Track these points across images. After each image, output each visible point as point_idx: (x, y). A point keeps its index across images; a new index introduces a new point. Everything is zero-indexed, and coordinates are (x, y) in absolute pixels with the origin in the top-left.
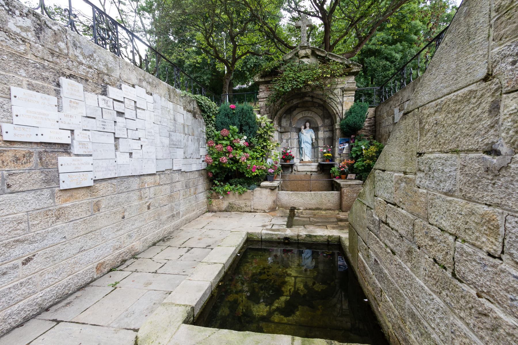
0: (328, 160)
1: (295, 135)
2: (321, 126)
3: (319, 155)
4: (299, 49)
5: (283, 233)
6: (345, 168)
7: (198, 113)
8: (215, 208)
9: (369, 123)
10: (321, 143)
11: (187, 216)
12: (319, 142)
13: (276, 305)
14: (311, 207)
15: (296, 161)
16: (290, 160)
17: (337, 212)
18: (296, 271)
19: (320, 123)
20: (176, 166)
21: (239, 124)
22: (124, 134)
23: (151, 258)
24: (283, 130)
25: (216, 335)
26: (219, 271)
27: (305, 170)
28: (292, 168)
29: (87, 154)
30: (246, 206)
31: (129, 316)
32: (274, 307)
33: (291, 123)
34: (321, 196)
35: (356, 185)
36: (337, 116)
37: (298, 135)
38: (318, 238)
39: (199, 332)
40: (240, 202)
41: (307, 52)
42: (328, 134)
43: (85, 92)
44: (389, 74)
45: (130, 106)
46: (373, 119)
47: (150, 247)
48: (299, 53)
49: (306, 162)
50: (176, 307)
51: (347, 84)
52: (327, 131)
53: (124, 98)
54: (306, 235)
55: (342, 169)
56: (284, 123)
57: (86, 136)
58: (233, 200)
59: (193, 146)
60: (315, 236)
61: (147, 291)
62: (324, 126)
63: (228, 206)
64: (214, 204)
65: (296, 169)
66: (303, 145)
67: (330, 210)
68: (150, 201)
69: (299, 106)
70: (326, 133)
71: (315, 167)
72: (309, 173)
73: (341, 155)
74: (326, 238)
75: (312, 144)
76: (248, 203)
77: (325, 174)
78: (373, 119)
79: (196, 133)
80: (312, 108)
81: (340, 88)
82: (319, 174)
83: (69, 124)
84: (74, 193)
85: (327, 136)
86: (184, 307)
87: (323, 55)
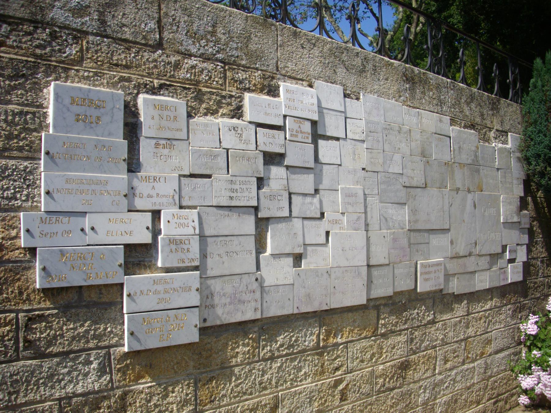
20: (426, 280)
22: (281, 208)
29: (187, 264)
43: (346, 99)
45: (300, 135)
53: (293, 284)
57: (186, 222)
68: (349, 377)
83: (150, 196)
84: (232, 208)
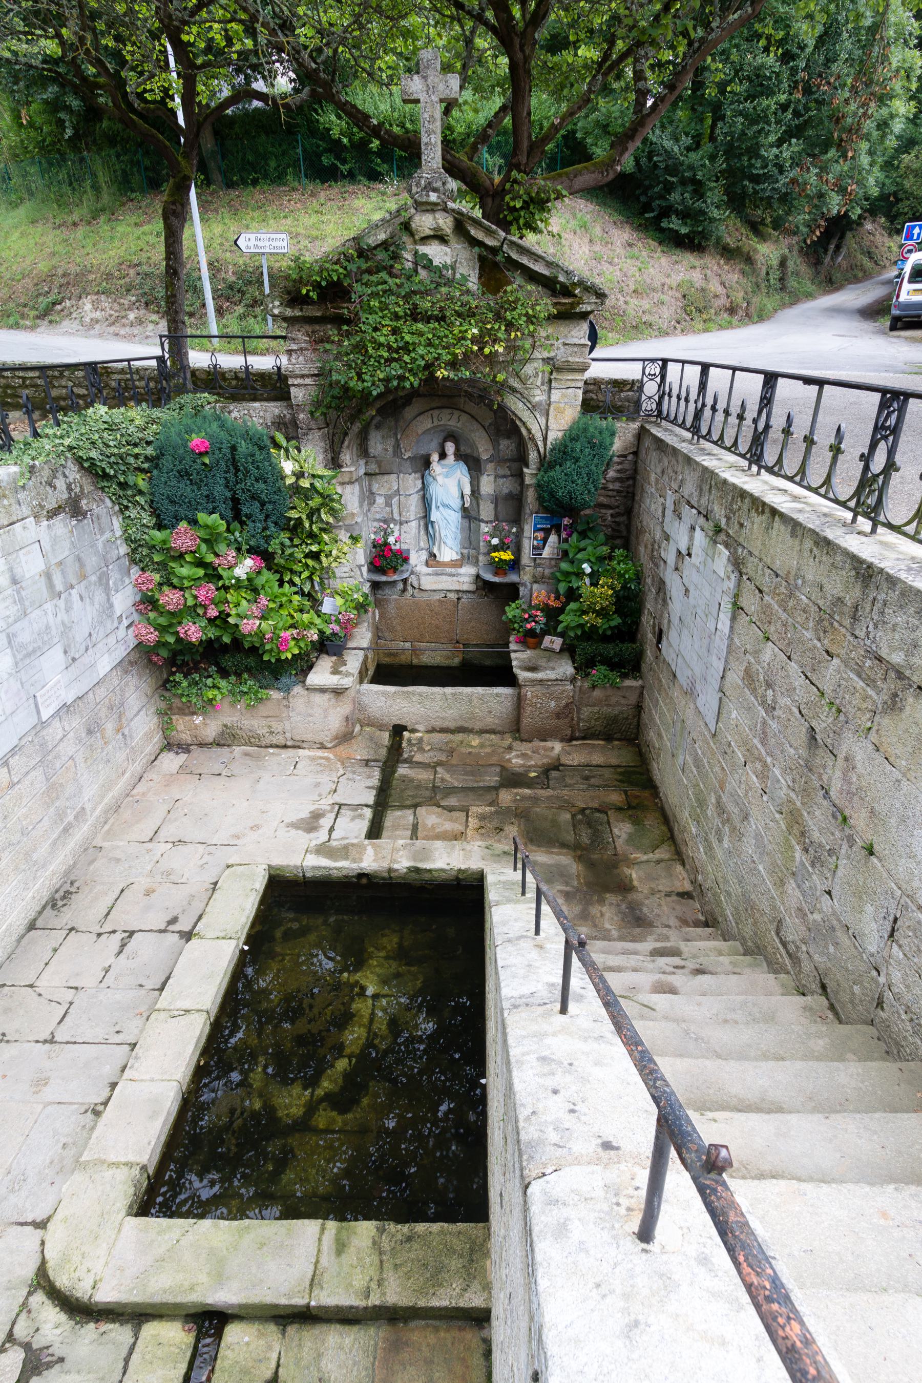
1: (412, 483)
2: (489, 461)
4: (413, 211)
5: (354, 866)
6: (536, 622)
7: (88, 488)
8: (186, 737)
9: (618, 471)
10: (487, 511)
11: (106, 800)
13: (326, 1085)
14: (444, 726)
15: (417, 559)
17: (508, 740)
18: (378, 976)
19: (484, 450)
21: (229, 495)
23: (31, 986)
24: (373, 468)
25: (189, 1236)
26: (195, 1040)
27: (440, 587)
30: (271, 733)
31: (17, 1188)
32: (320, 1092)
33: (397, 447)
34: (470, 701)
35: (557, 680)
36: (530, 445)
37: (423, 477)
38: (436, 874)
39: (159, 1233)
40: (255, 723)
41: (441, 222)
42: (507, 486)
44: (769, 106)
46: (630, 457)
47: (23, 936)
48: (413, 225)
49: (445, 565)
50: (111, 1172)
51: (562, 349)
52: (504, 476)
54: (408, 868)
55: (528, 626)
56: (378, 445)
58: (235, 719)
59: (88, 608)
60: (430, 871)
61: (41, 1106)
62: (497, 459)
63: (223, 733)
64: (181, 727)
65: (416, 584)
66: (435, 516)
67: (492, 732)
70: (501, 481)
71: (467, 579)
74: (455, 873)
75: (464, 510)
76: (276, 726)
78: (630, 457)
79: (92, 562)
82: (481, 596)
85: (506, 491)
86: (125, 1169)
87: (490, 242)
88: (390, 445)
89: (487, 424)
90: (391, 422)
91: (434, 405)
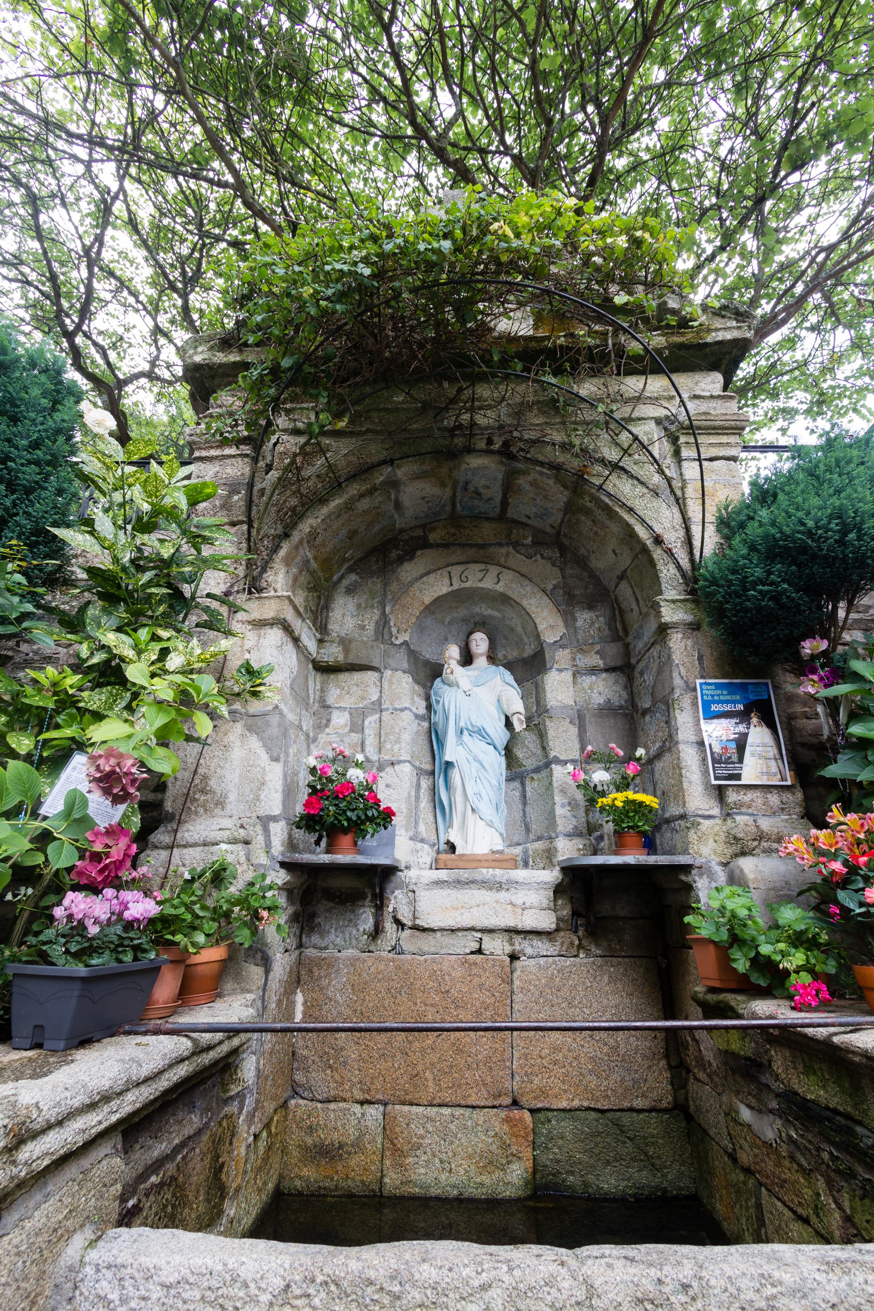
0: (632, 838)
2: (559, 644)
3: (560, 811)
12: (551, 733)
16: (357, 828)
24: (333, 653)
27: (466, 921)
28: (380, 904)
33: (383, 623)
36: (657, 554)
37: (428, 698)
49: (476, 861)
52: (593, 671)
69: (433, 537)
70: (587, 681)
71: (544, 897)
72: (496, 946)
73: (732, 797)
77: (610, 954)
80: (503, 550)
81: (658, 421)
85: (598, 699)
88: (370, 620)
89: (550, 587)
90: (376, 584)
91: (452, 560)
